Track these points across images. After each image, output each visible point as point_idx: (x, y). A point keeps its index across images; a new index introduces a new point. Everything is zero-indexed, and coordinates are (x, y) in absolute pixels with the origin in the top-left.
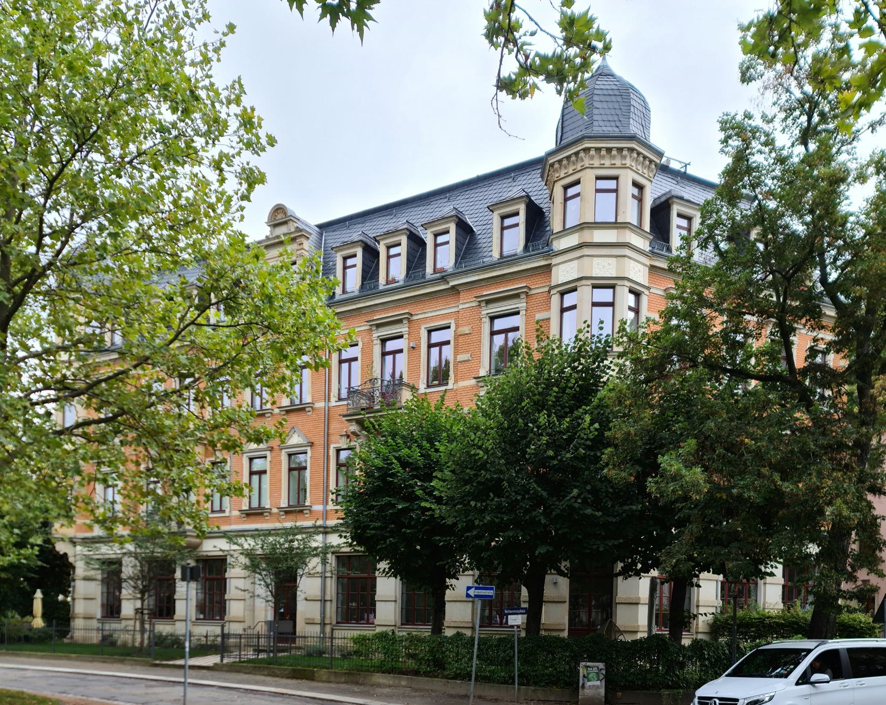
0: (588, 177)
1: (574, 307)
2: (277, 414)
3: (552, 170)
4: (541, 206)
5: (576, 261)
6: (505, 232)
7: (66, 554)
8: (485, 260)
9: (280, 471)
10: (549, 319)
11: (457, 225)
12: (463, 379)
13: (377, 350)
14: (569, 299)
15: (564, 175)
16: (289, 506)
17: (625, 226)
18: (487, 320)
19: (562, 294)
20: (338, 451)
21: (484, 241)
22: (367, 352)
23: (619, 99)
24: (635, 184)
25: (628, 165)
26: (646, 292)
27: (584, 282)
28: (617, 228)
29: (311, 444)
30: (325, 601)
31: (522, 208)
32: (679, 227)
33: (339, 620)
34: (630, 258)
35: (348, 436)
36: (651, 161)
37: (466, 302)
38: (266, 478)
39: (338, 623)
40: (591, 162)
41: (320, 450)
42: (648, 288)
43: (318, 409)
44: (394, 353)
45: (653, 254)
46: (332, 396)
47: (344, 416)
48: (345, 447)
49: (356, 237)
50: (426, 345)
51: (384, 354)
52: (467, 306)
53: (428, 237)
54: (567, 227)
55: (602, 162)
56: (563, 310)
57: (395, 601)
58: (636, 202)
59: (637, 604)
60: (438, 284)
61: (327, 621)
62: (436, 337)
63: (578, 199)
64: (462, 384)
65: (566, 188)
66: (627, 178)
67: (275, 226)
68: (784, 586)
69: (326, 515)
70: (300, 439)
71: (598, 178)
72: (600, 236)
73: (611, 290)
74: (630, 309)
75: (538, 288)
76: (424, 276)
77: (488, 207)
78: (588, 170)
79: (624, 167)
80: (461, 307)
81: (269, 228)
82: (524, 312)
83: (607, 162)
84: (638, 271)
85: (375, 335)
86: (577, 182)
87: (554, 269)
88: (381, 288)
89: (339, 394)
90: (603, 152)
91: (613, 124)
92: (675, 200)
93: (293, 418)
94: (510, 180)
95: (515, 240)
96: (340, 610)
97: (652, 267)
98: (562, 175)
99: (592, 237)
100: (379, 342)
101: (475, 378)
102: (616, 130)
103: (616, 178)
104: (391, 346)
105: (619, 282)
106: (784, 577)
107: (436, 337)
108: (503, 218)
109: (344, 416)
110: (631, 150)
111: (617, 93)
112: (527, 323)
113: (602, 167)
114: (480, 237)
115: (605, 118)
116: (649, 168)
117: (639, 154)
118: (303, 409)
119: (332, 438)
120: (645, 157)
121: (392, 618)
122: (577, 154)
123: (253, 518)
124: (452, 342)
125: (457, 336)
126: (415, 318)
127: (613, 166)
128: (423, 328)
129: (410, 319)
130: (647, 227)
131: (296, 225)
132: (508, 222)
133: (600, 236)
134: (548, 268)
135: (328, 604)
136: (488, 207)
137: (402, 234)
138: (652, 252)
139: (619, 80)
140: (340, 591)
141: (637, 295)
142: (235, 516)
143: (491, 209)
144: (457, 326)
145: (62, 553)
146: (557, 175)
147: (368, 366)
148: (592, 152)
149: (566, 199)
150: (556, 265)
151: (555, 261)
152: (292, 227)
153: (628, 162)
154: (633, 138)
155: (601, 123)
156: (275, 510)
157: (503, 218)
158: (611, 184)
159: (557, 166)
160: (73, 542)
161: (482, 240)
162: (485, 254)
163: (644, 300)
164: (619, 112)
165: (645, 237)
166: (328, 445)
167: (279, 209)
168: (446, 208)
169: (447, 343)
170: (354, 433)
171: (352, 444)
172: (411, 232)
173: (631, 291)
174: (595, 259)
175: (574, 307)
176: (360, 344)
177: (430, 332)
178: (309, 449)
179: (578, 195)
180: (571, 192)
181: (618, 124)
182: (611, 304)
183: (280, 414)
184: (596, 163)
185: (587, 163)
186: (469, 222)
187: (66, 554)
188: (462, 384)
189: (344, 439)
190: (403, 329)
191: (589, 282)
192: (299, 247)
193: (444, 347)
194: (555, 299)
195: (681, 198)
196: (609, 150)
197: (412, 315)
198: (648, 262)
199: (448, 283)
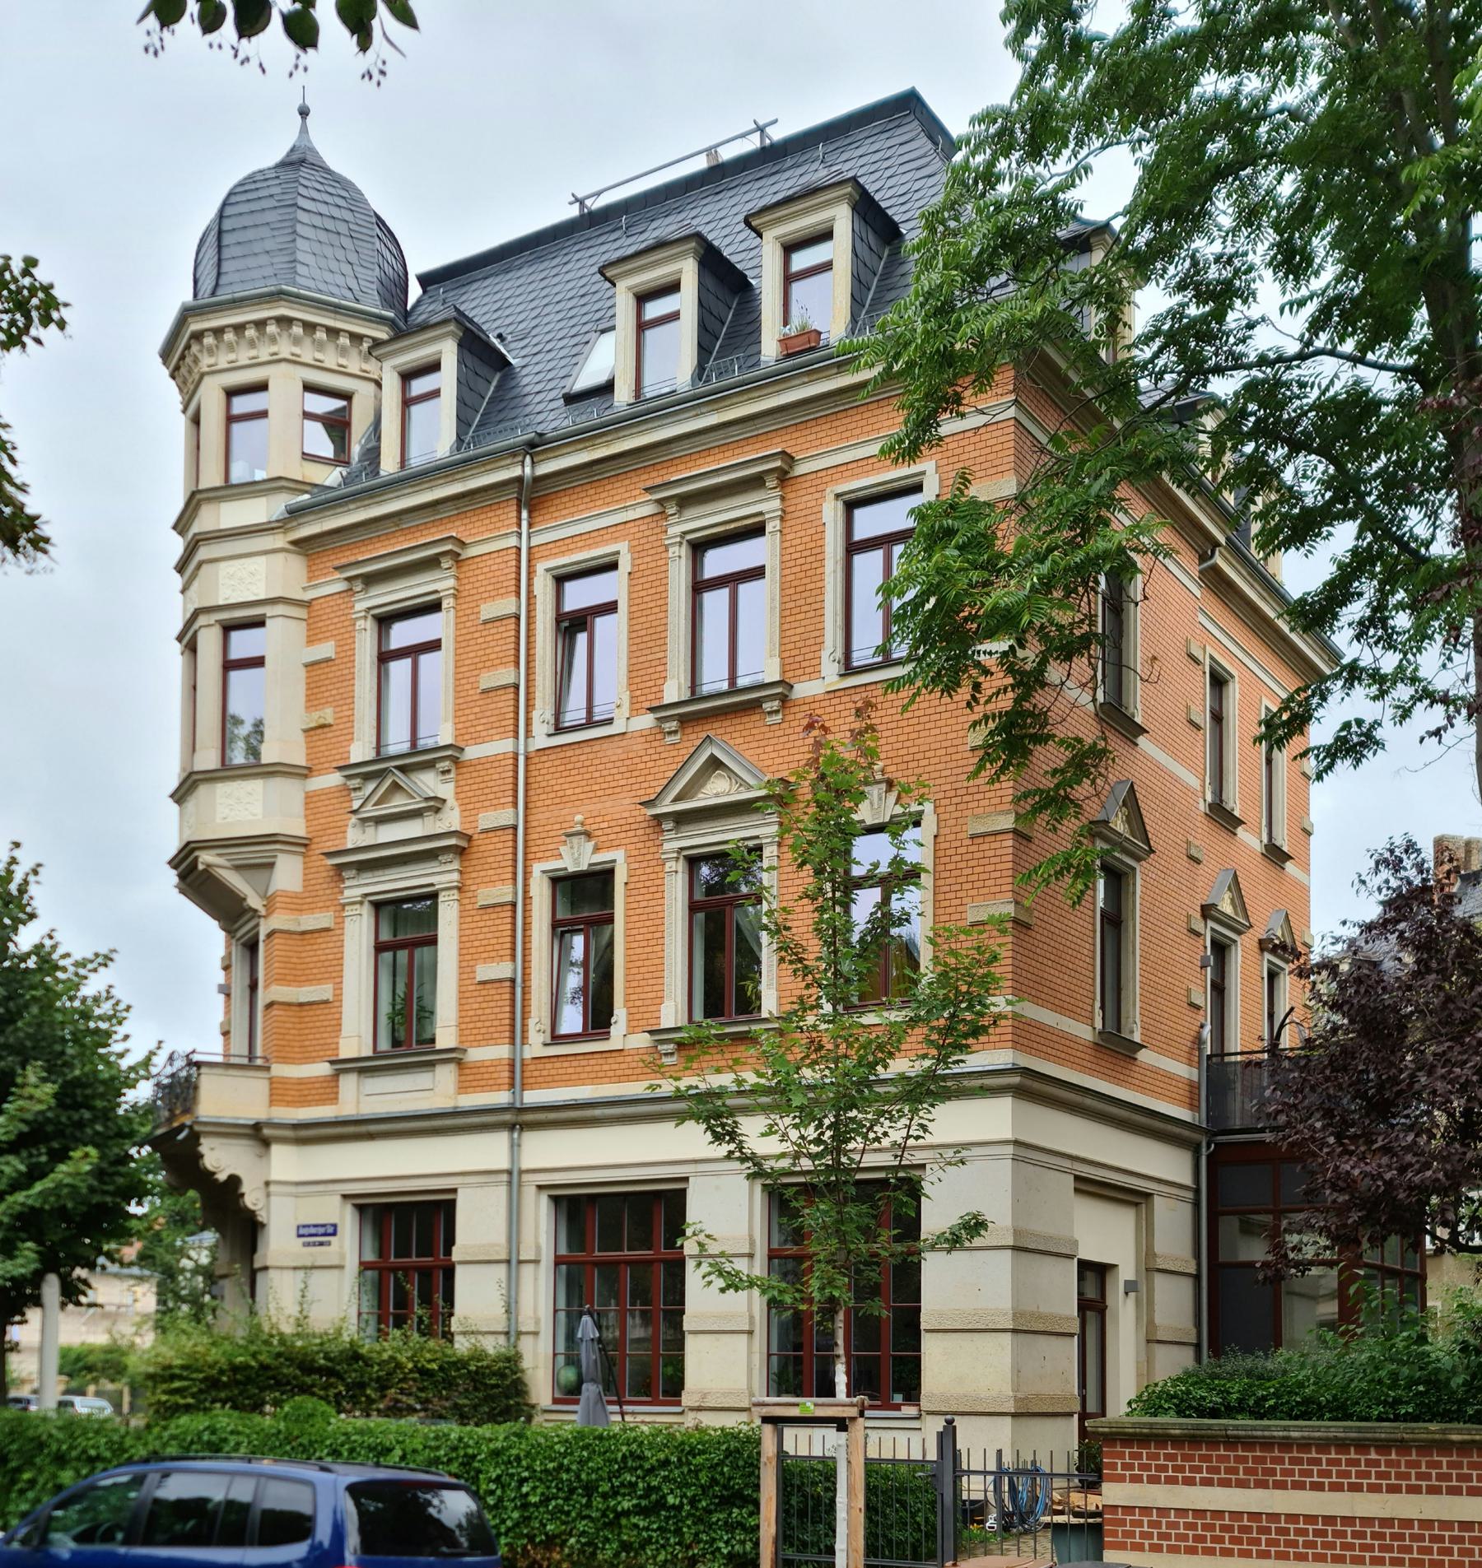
1: (258, 662)
5: (263, 559)
6: (796, 287)
7: (234, 1181)
11: (855, 209)
14: (244, 644)
18: (370, 625)
19: (228, 628)
22: (648, 584)
44: (414, 652)
51: (385, 657)
57: (750, 1333)
62: (579, 595)
77: (601, 271)
85: (672, 531)
86: (262, 387)
89: (558, 713)
98: (223, 365)
100: (684, 551)
101: (652, 710)
104: (403, 634)
108: (790, 248)
121: (742, 1383)
126: (463, 557)
137: (838, 200)
145: (222, 1177)
157: (790, 248)
160: (259, 1135)
172: (467, 331)
175: (258, 662)
177: (561, 580)
181: (353, 258)
187: (234, 1181)
193: (424, 659)
197: (463, 544)
198: (279, 541)
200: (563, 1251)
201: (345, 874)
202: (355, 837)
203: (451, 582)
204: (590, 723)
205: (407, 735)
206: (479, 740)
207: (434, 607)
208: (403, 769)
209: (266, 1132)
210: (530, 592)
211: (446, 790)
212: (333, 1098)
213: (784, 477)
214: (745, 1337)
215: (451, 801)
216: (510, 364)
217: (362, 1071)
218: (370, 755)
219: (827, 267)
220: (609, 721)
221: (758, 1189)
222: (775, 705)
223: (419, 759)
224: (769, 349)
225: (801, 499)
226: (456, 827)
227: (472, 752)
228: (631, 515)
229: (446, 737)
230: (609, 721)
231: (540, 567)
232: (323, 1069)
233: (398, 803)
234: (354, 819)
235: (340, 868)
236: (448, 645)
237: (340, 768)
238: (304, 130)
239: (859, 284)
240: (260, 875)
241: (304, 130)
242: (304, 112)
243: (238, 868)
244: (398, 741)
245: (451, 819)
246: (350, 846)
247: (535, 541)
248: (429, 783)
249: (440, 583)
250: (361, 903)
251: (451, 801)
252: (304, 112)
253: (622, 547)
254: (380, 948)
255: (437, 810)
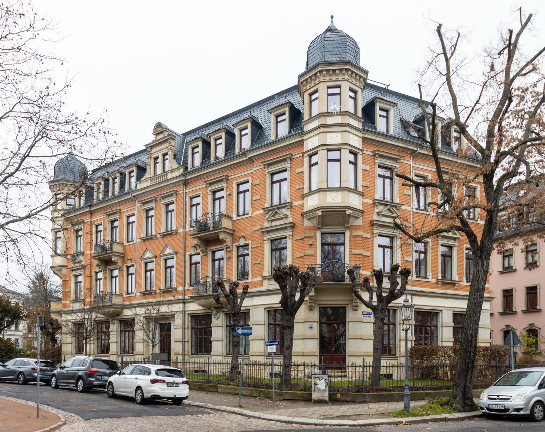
0: (322, 87)
1: (317, 163)
2: (159, 238)
3: (302, 86)
4: (300, 109)
8: (268, 141)
9: (160, 269)
10: (304, 172)
12: (257, 210)
13: (210, 197)
14: (314, 159)
15: (309, 88)
16: (166, 288)
17: (347, 113)
18: (269, 175)
19: (310, 156)
20: (191, 256)
21: (268, 131)
22: (205, 200)
23: (340, 42)
24: (351, 90)
25: (346, 79)
26: (361, 153)
27: (321, 148)
28: (340, 115)
29: (176, 253)
30: (185, 342)
31: (287, 110)
32: (380, 116)
33: (193, 352)
34: (349, 132)
35: (196, 247)
36: (361, 77)
37: (257, 167)
38: (174, 270)
39: (192, 354)
40: (331, 78)
41: (181, 255)
42: (362, 151)
43: (180, 233)
44: (280, 181)
45: (364, 130)
46: (187, 224)
47: (192, 235)
48: (194, 253)
49: (198, 136)
50: (236, 192)
52: (258, 168)
53: (236, 132)
54: (313, 115)
55: (331, 78)
56: (311, 166)
58: (352, 101)
59: (286, 238)
60: (241, 157)
61: (186, 353)
63: (317, 100)
64: (256, 213)
65: (311, 95)
66: (346, 86)
67: (157, 135)
68: (454, 328)
69: (184, 292)
70: (170, 250)
71: (329, 87)
72: (330, 120)
73: (339, 152)
74: (351, 162)
75: (297, 154)
76: (234, 154)
77: (268, 111)
78: (322, 83)
79: (344, 80)
80: (254, 169)
81: (154, 136)
82: (289, 169)
83: (334, 78)
84: (356, 141)
86: (316, 91)
87: (305, 142)
88: (212, 162)
90: (331, 72)
91: (336, 56)
92: (377, 100)
93: (168, 239)
94: (284, 98)
95: (284, 129)
96: (194, 347)
97: (364, 139)
98: (308, 88)
99: (326, 121)
101: (262, 209)
102: (339, 59)
103: (339, 87)
105: (343, 147)
106: (453, 322)
107: (242, 188)
108: (277, 117)
109: (192, 235)
110: (348, 70)
111: (338, 38)
112: (291, 176)
113: (331, 81)
114: (266, 129)
115: (332, 53)
116: (360, 81)
117: (352, 72)
118: (172, 234)
119: (187, 249)
120: (357, 74)
122: (315, 74)
123: (147, 296)
124: (250, 190)
125: (253, 186)
127: (337, 80)
128: (234, 183)
129: (227, 179)
130: (360, 114)
131: (168, 133)
132: (280, 119)
133: (330, 120)
134: (302, 141)
135: (186, 343)
136: (268, 111)
138: (363, 129)
139: (340, 32)
140: (194, 336)
141: (355, 155)
142: (138, 296)
143: (270, 112)
144: (253, 181)
146: (305, 88)
147: (205, 207)
148: (324, 73)
149: (311, 102)
150: (306, 140)
151: (305, 137)
152: (165, 134)
153: (346, 77)
154: (348, 63)
155: (329, 56)
156: (158, 291)
157: (277, 117)
158: (337, 91)
159: (304, 83)
161: (267, 131)
162: (268, 138)
163: (360, 157)
164: (340, 49)
165: (359, 121)
166: (185, 253)
167: (159, 125)
168: (247, 115)
169: (248, 190)
170: (197, 245)
171: (197, 251)
172: (227, 130)
173: (351, 152)
174: (328, 134)
175: (317, 163)
176: (201, 195)
178: (175, 255)
179: (317, 98)
180: (313, 97)
181: (340, 56)
182: (339, 160)
183: (160, 237)
184: (327, 78)
185: (322, 79)
186: (260, 122)
188: (256, 213)
189: (193, 249)
190: (224, 185)
191: (325, 148)
192: (169, 145)
194: (306, 159)
195: (382, 99)
196: (334, 71)
197: (228, 176)
198: (361, 135)
199: (247, 156)
200: (194, 326)
201: (265, 233)
202: (266, 224)
203: (175, 199)
204: (244, 214)
205: (243, 210)
206: (296, 201)
207: (285, 170)
208: (278, 208)
209: (61, 312)
210: (185, 201)
211: (288, 213)
212: (262, 285)
213: (291, 159)
214: (221, 342)
215: (290, 215)
216: (262, 127)
217: (269, 279)
218: (270, 206)
219: (284, 120)
220: (248, 214)
221: (189, 317)
222: (289, 207)
223: (281, 206)
224: (237, 150)
225: (179, 197)
226: (291, 221)
227: (295, 204)
228: (102, 217)
229: (288, 200)
230: (248, 214)
231: (187, 196)
232: (259, 279)
233: (277, 216)
234: (266, 220)
235: (263, 232)
236: (288, 179)
237: (262, 209)
238: (332, 22)
239: (226, 146)
240: (61, 271)
241: (332, 22)
242: (332, 17)
243: (58, 270)
244: (276, 201)
245: (290, 220)
246: (265, 227)
247: (186, 191)
248: (285, 211)
249: (287, 165)
250: (268, 240)
251: (290, 215)
252: (332, 17)
253: (102, 221)
254: (272, 250)
255: (286, 218)
